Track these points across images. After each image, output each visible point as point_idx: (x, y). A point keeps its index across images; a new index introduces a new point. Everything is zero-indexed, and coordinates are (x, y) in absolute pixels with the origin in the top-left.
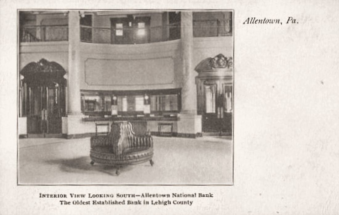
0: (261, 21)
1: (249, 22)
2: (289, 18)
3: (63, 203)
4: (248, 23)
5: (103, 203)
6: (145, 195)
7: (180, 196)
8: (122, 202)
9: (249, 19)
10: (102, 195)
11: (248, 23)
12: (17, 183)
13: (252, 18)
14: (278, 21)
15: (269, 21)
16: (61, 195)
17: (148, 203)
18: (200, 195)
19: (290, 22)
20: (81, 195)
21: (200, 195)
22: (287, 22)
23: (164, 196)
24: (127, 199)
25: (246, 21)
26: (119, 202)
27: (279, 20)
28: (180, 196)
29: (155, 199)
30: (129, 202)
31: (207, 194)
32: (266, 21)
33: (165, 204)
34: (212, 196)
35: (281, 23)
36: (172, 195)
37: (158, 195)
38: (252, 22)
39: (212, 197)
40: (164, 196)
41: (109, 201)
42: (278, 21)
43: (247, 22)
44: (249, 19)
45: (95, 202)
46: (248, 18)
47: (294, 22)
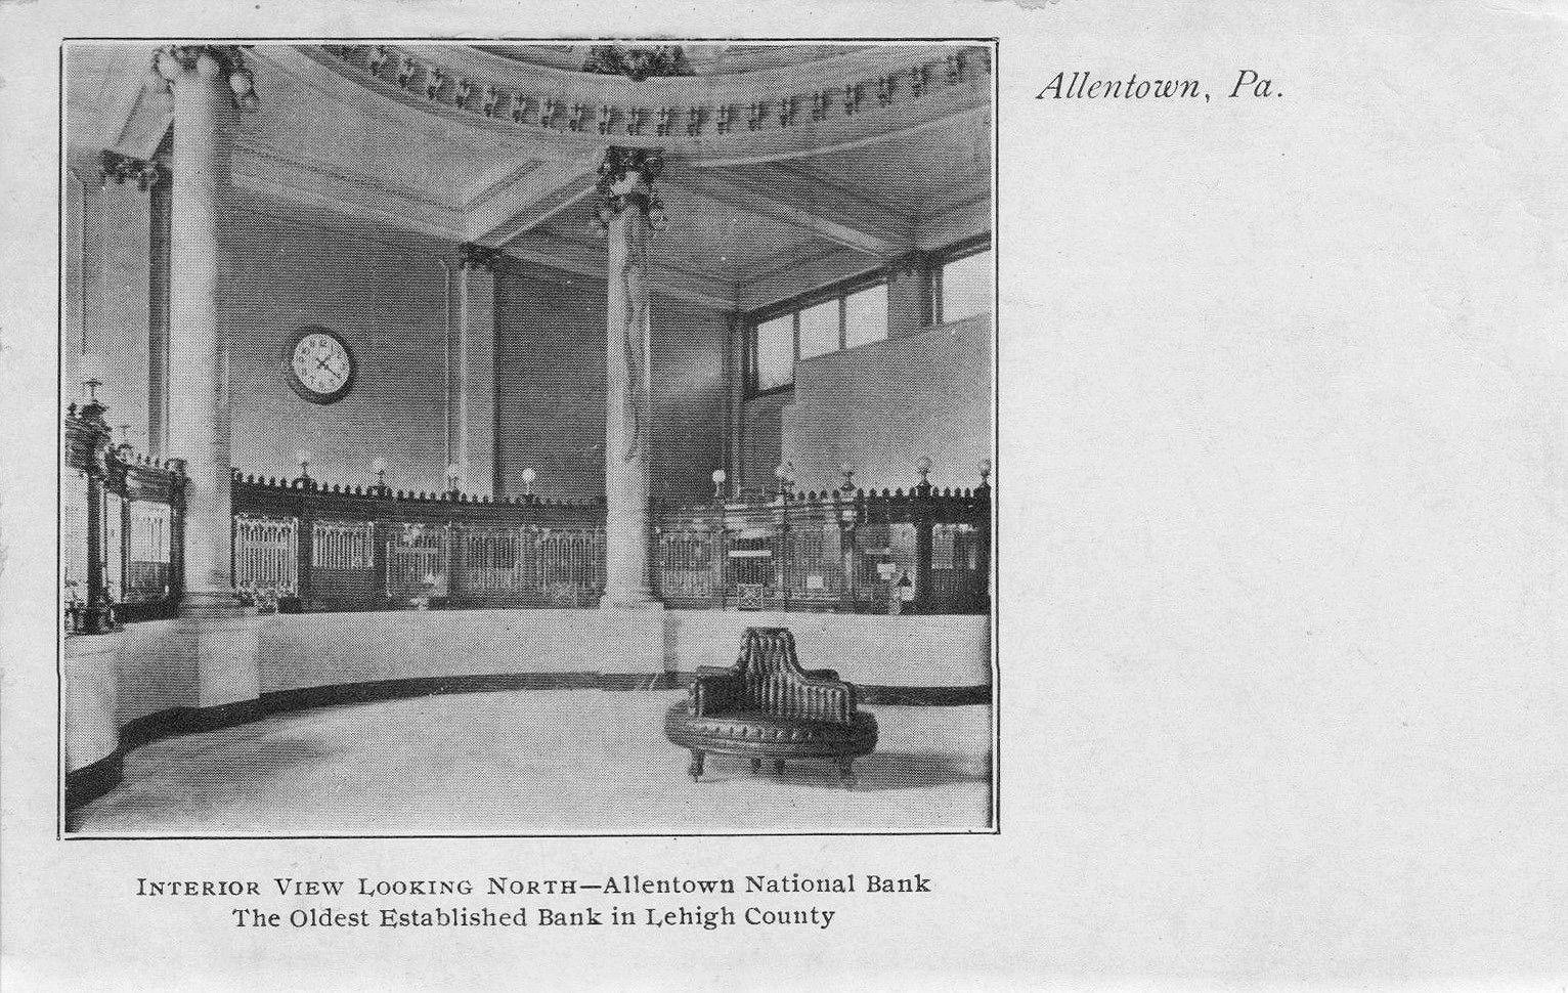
3: (249, 919)
6: (621, 885)
7: (780, 885)
11: (1058, 96)
14: (1191, 88)
17: (629, 918)
18: (876, 885)
19: (1246, 91)
21: (876, 885)
23: (708, 886)
24: (738, 902)
28: (780, 885)
29: (663, 903)
33: (710, 924)
34: (926, 885)
38: (1085, 92)
39: (926, 890)
42: (1191, 88)
44: (1061, 76)
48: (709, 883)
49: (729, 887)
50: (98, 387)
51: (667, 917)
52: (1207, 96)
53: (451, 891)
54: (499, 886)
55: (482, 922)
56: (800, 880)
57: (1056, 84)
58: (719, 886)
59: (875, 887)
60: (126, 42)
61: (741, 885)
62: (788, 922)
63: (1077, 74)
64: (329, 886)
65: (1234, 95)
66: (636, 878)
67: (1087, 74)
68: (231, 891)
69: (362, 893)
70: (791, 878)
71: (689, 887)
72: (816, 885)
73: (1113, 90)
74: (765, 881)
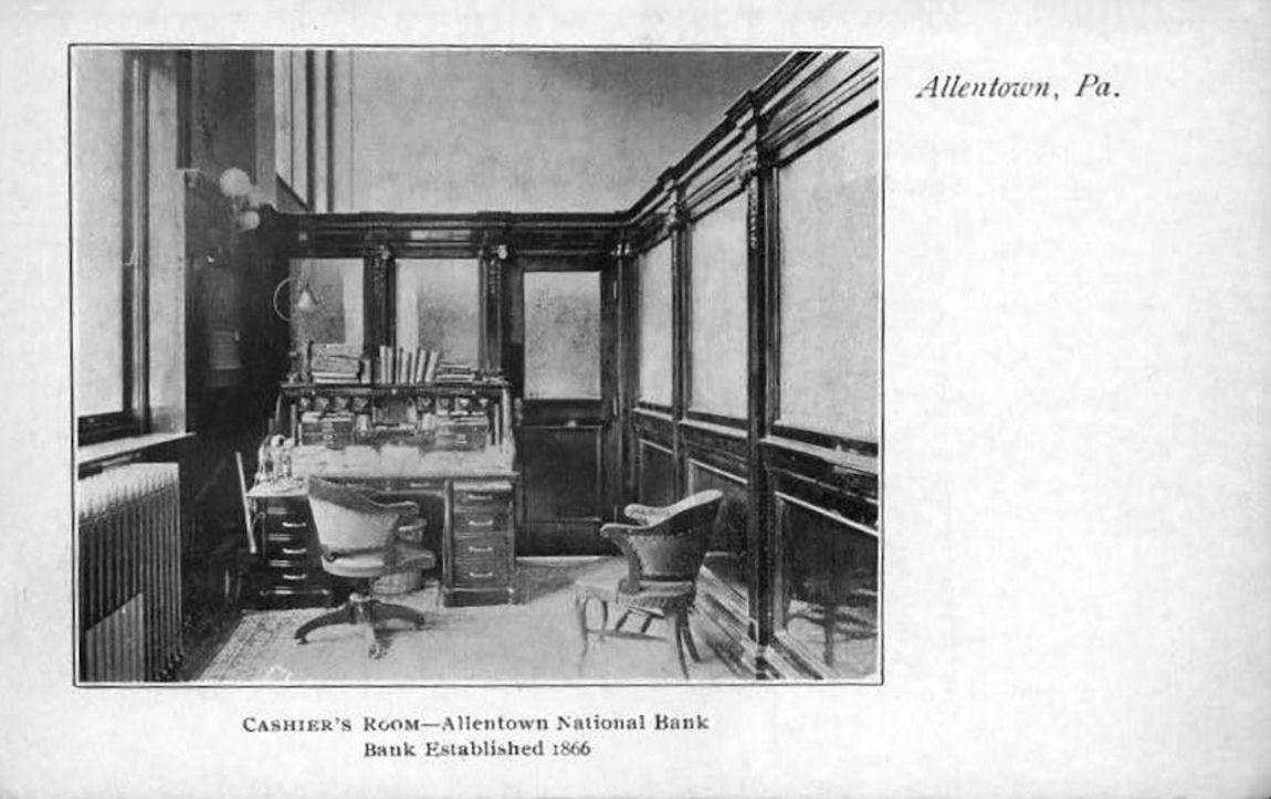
0: (980, 87)
1: (938, 92)
2: (1087, 77)
4: (934, 95)
5: (464, 752)
6: (456, 723)
8: (532, 746)
9: (936, 78)
10: (317, 722)
11: (934, 95)
12: (876, 685)
13: (949, 78)
14: (1043, 89)
15: (1012, 89)
16: (510, 720)
18: (660, 722)
19: (1089, 91)
20: (521, 722)
22: (1079, 94)
23: (526, 725)
24: (552, 737)
25: (926, 88)
26: (521, 747)
27: (1047, 85)
30: (370, 747)
31: (688, 717)
32: (1001, 88)
35: (1056, 95)
36: (557, 721)
37: (505, 719)
40: (526, 725)
41: (486, 743)
42: (1043, 89)
43: (930, 92)
44: (936, 78)
45: (432, 746)
46: (933, 78)
47: (1105, 93)
49: (542, 724)
52: (1056, 95)
56: (600, 720)
57: (932, 85)
58: (535, 725)
60: (73, 74)
61: (553, 723)
62: (556, 746)
63: (949, 78)
65: (1079, 94)
66: (468, 718)
67: (958, 77)
70: (592, 719)
71: (511, 725)
73: (979, 90)
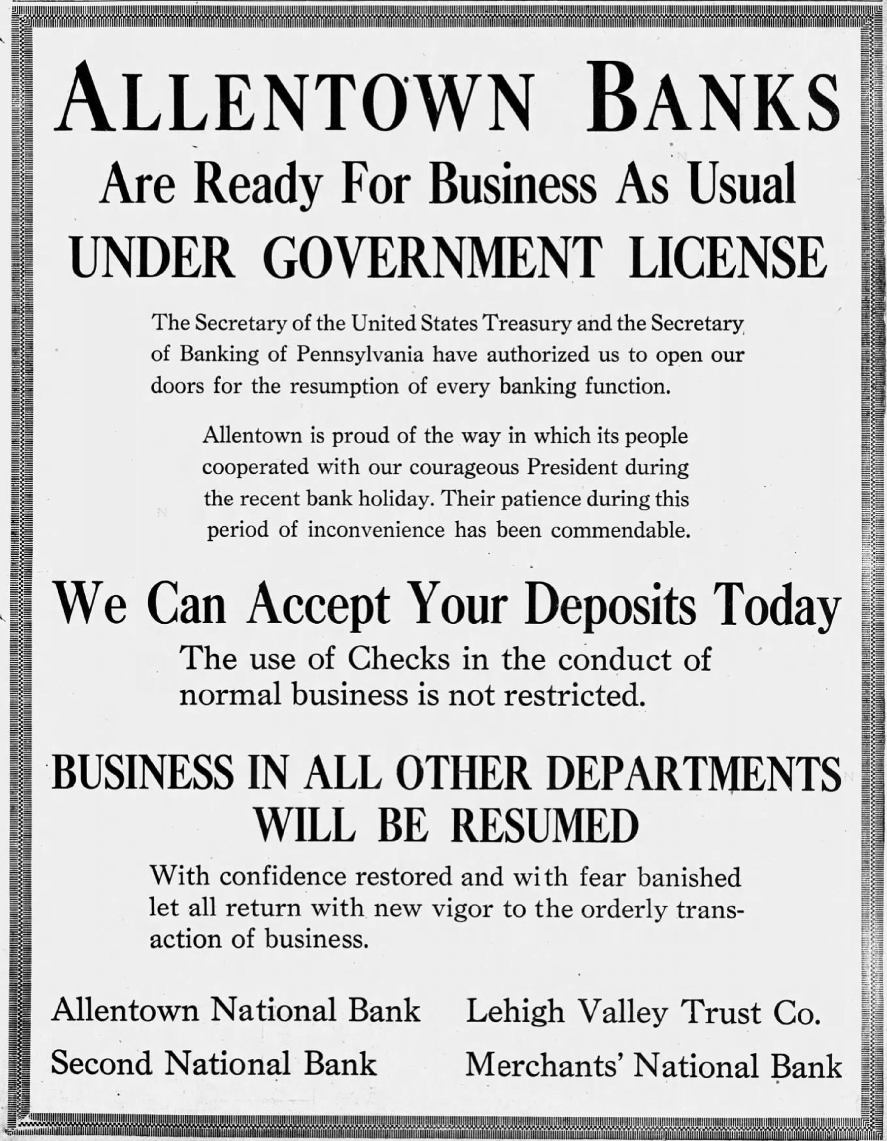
7: (255, 1012)
28: (255, 1012)
48: (169, 1008)
50: (602, 690)
51: (438, 388)
53: (378, 359)
54: (645, 1061)
55: (700, 883)
59: (360, 1014)
64: (409, 908)
68: (515, 913)
69: (472, 1019)
71: (148, 1013)
72: (248, 1066)
74: (601, 1006)
